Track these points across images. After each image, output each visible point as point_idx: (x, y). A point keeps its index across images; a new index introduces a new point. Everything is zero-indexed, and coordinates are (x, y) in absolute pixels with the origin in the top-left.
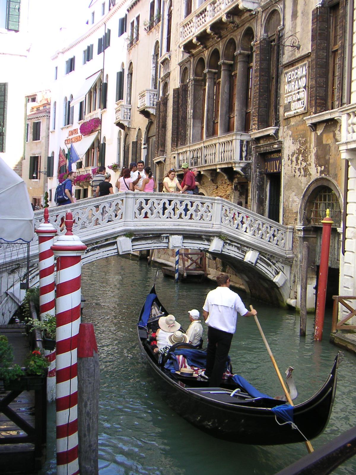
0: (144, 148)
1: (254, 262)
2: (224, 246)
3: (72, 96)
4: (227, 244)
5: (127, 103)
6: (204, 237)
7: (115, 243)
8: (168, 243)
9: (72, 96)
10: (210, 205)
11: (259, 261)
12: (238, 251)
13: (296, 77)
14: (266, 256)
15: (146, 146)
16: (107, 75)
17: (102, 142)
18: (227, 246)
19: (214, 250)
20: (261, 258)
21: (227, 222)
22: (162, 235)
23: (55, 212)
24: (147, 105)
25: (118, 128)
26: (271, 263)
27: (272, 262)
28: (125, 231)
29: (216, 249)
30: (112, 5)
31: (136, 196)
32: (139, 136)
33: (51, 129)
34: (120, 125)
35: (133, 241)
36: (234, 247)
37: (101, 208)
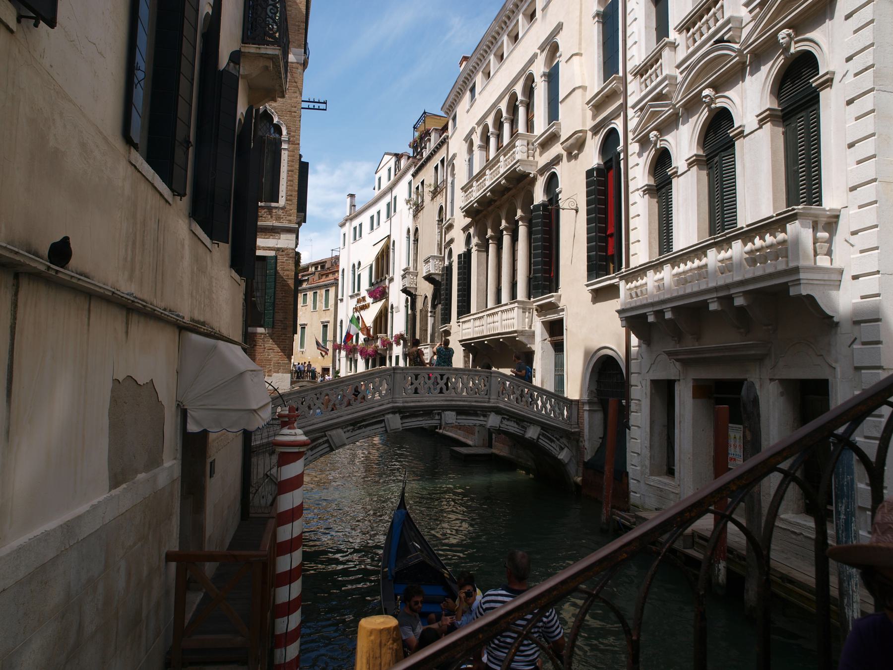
0: (431, 316)
1: (535, 437)
2: (501, 422)
3: (359, 263)
6: (479, 412)
7: (383, 421)
8: (440, 419)
9: (359, 263)
11: (541, 437)
12: (517, 426)
16: (394, 241)
18: (505, 422)
20: (543, 434)
25: (404, 296)
27: (556, 438)
28: (393, 408)
33: (340, 297)
34: (405, 291)
35: (402, 418)
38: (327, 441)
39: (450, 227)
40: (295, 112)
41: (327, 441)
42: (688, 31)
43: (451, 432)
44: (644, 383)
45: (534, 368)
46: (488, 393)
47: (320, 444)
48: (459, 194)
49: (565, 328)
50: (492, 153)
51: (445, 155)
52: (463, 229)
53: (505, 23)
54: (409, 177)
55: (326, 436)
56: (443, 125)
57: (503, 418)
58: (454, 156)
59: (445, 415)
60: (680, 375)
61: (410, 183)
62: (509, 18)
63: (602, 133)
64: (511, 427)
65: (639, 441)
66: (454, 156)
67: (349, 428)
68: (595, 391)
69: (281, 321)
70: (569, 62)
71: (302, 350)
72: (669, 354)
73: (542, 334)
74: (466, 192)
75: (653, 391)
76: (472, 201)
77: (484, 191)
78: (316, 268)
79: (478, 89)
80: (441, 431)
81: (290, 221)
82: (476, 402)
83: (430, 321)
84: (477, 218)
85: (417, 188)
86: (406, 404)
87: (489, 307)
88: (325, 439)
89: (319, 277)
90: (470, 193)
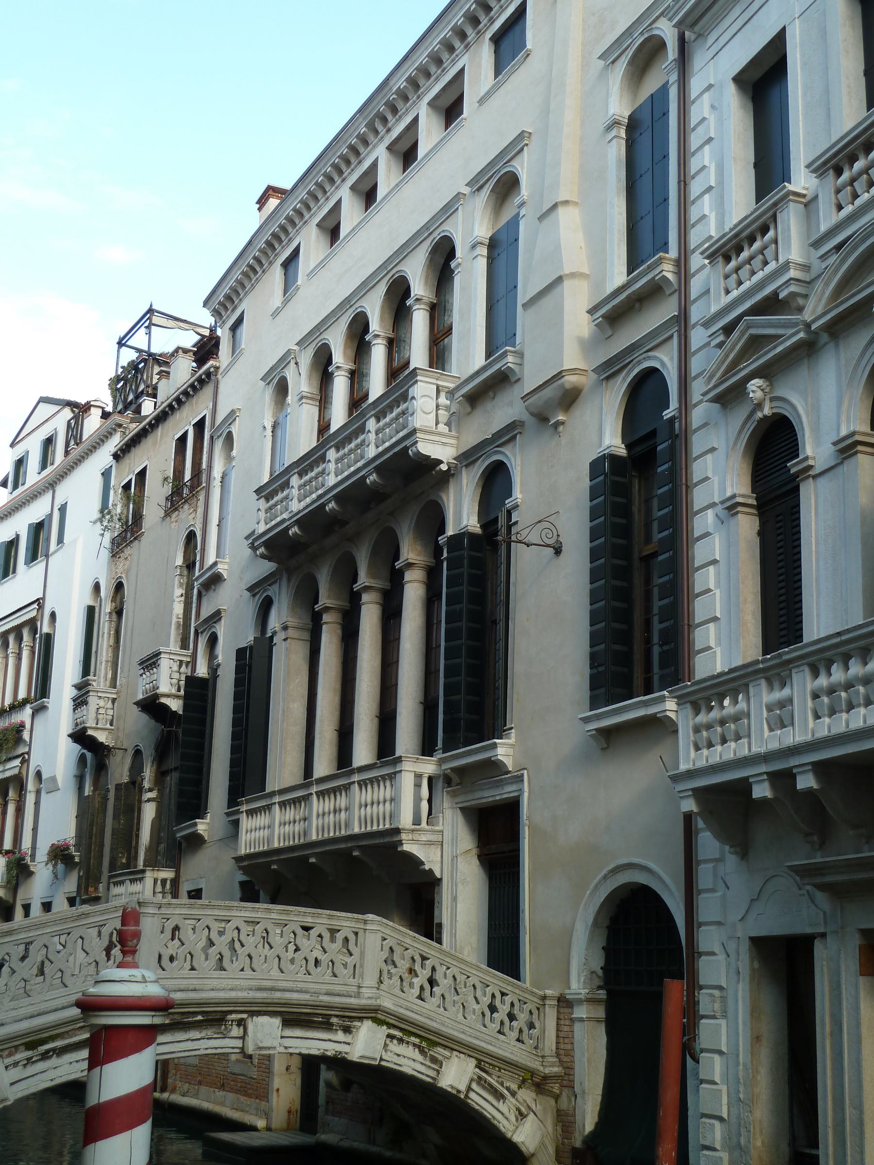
1: (463, 1087)
2: (386, 1045)
4: (395, 1041)
5: (105, 685)
6: (334, 1020)
8: (243, 1038)
10: (352, 937)
11: (474, 1086)
12: (420, 1058)
14: (491, 1071)
18: (394, 1046)
19: (362, 1057)
20: (480, 1078)
21: (396, 980)
27: (508, 1089)
29: (367, 1054)
30: (72, 442)
31: (163, 911)
32: (136, 768)
39: (216, 580)
42: (839, 172)
43: (196, 1096)
44: (732, 946)
45: (436, 921)
50: (338, 416)
51: (207, 412)
52: (250, 589)
53: (384, 120)
54: (103, 457)
56: (413, 142)
57: (389, 1036)
58: (232, 416)
60: (825, 923)
61: (106, 474)
62: (394, 110)
66: (232, 416)
68: (600, 972)
70: (546, 222)
72: (804, 872)
74: (267, 499)
75: (756, 965)
76: (284, 521)
77: (320, 497)
79: (304, 264)
80: (165, 1095)
83: (149, 812)
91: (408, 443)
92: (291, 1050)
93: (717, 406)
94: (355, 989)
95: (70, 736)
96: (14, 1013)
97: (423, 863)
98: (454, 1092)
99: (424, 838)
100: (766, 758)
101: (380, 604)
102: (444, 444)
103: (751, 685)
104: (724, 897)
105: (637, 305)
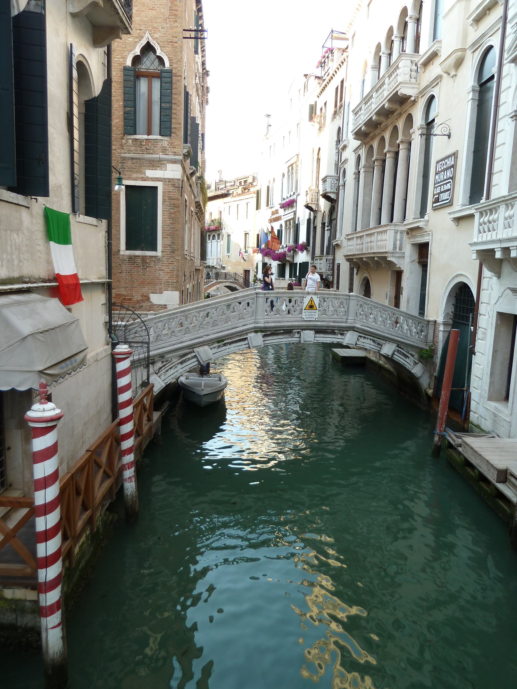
0: (327, 230)
2: (358, 339)
4: (362, 338)
6: (336, 331)
7: (246, 339)
8: (300, 337)
11: (396, 353)
12: (373, 344)
13: (445, 167)
15: (329, 228)
17: (297, 223)
18: (362, 340)
19: (347, 344)
20: (398, 350)
22: (293, 331)
23: (187, 312)
24: (328, 190)
25: (308, 211)
26: (409, 355)
27: (411, 354)
28: (255, 328)
29: (349, 343)
35: (264, 336)
36: (369, 340)
37: (231, 307)
38: (195, 356)
39: (345, 147)
40: (176, 43)
41: (195, 356)
45: (402, 286)
46: (347, 312)
47: (189, 359)
48: (352, 116)
49: (429, 252)
55: (194, 352)
59: (304, 334)
63: (481, 50)
64: (367, 345)
65: (481, 367)
67: (215, 345)
69: (170, 245)
71: (228, 254)
73: (411, 257)
75: (499, 322)
76: (360, 124)
77: (371, 114)
78: (240, 183)
81: (175, 154)
82: (334, 322)
84: (366, 141)
85: (321, 109)
86: (267, 325)
87: (357, 231)
88: (193, 354)
89: (242, 191)
90: (360, 116)
91: (397, 89)
92: (319, 341)
93: (513, 65)
94: (345, 320)
95: (304, 206)
96: (212, 331)
97: (396, 265)
98: (387, 355)
99: (397, 255)
100: (500, 241)
101: (394, 158)
102: (413, 88)
103: (500, 207)
104: (490, 293)
105: (488, 12)
